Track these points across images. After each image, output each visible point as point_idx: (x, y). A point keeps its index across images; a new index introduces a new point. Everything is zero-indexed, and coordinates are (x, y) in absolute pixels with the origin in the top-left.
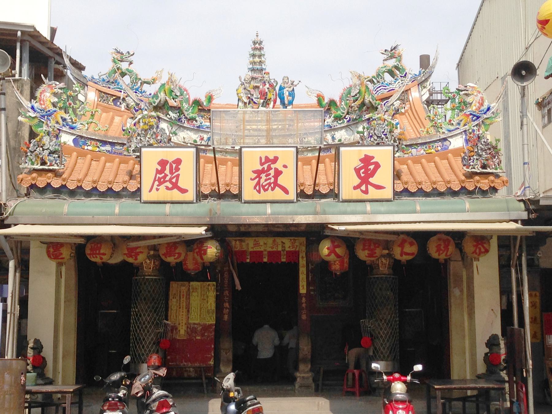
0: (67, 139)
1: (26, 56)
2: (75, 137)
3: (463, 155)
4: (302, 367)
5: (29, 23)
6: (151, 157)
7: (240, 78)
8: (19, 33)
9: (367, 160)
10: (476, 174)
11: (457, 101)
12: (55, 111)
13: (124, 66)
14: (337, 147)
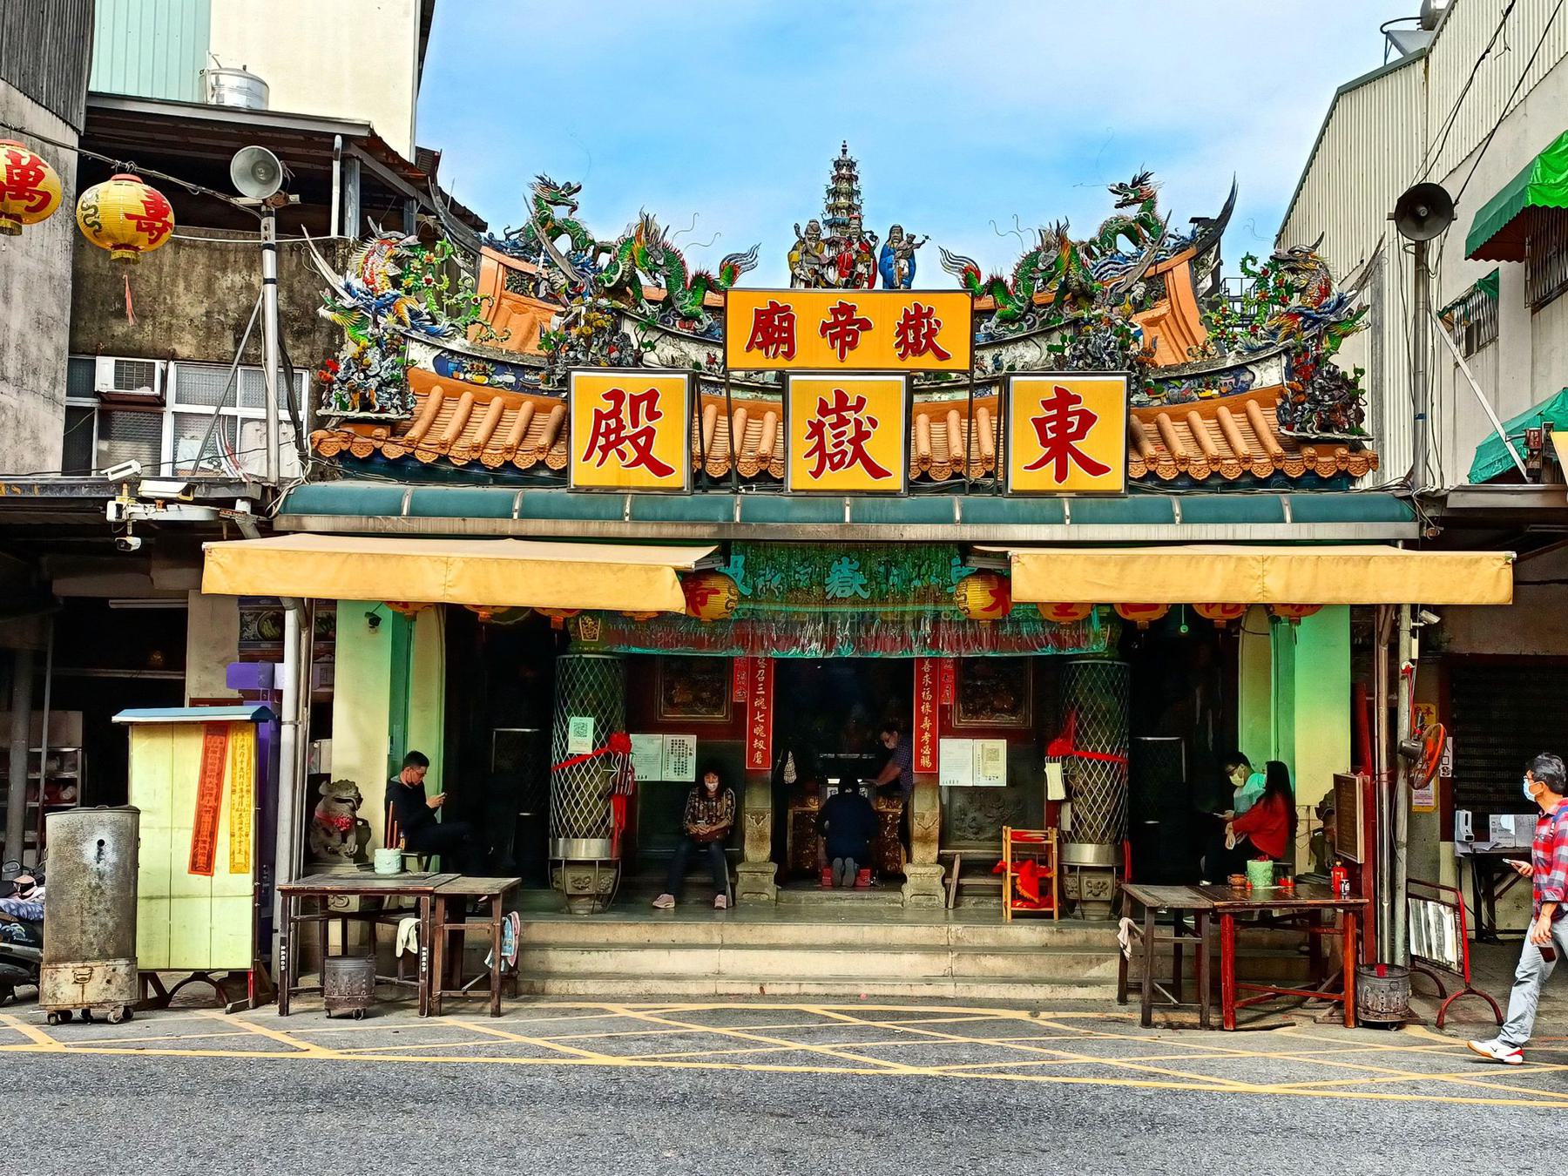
0: (421, 356)
1: (354, 191)
2: (437, 352)
3: (1279, 401)
4: (918, 852)
5: (359, 117)
6: (589, 389)
7: (797, 227)
8: (338, 140)
9: (1064, 399)
10: (1308, 442)
11: (1271, 283)
12: (396, 297)
13: (560, 213)
14: (1003, 383)
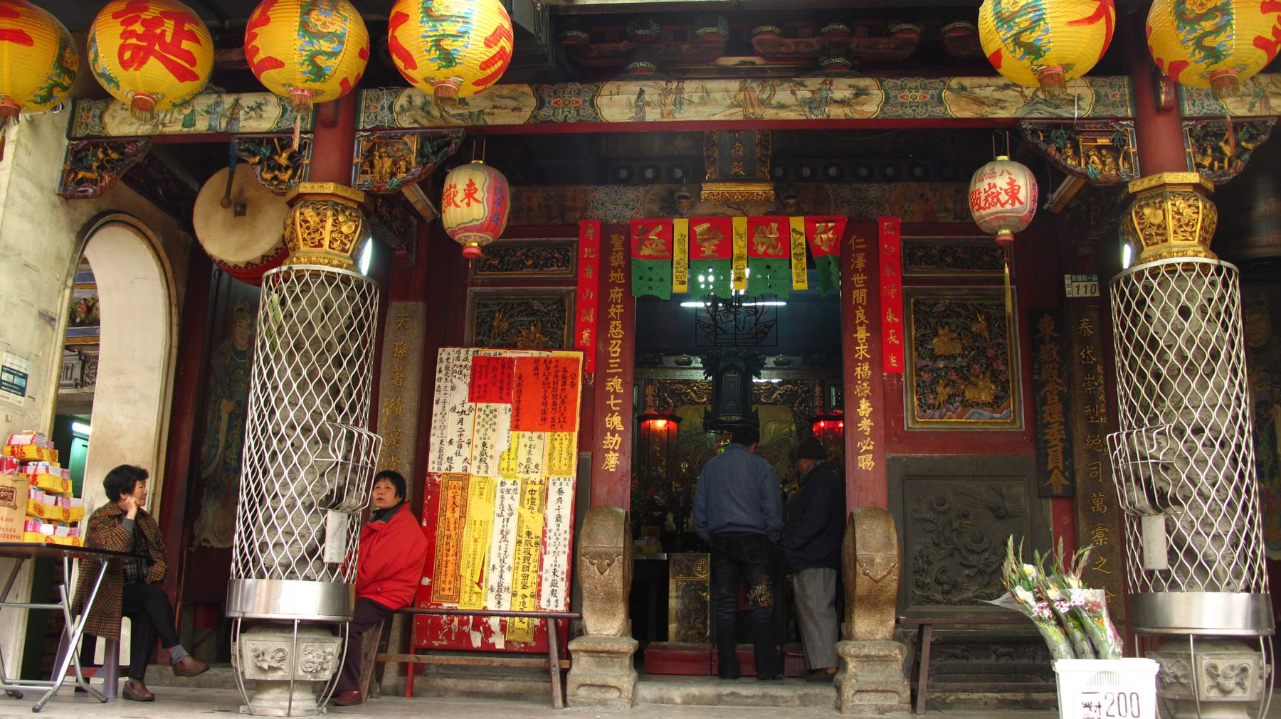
4: (863, 624)
